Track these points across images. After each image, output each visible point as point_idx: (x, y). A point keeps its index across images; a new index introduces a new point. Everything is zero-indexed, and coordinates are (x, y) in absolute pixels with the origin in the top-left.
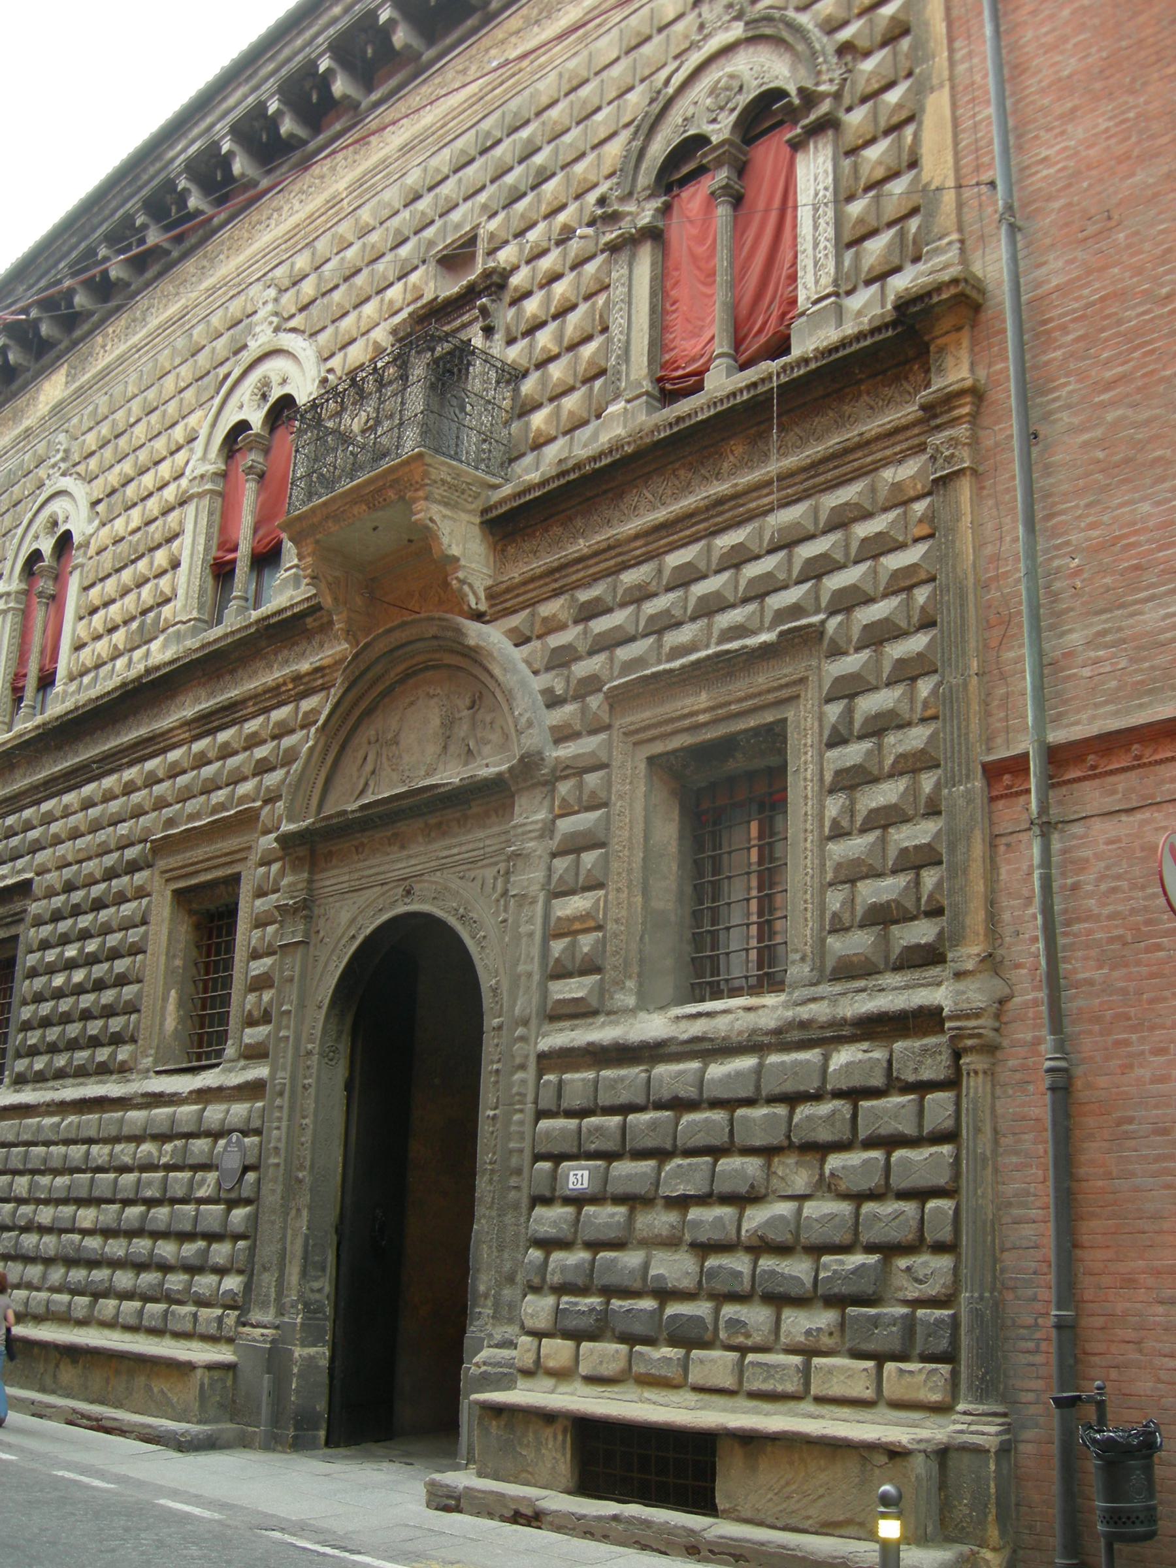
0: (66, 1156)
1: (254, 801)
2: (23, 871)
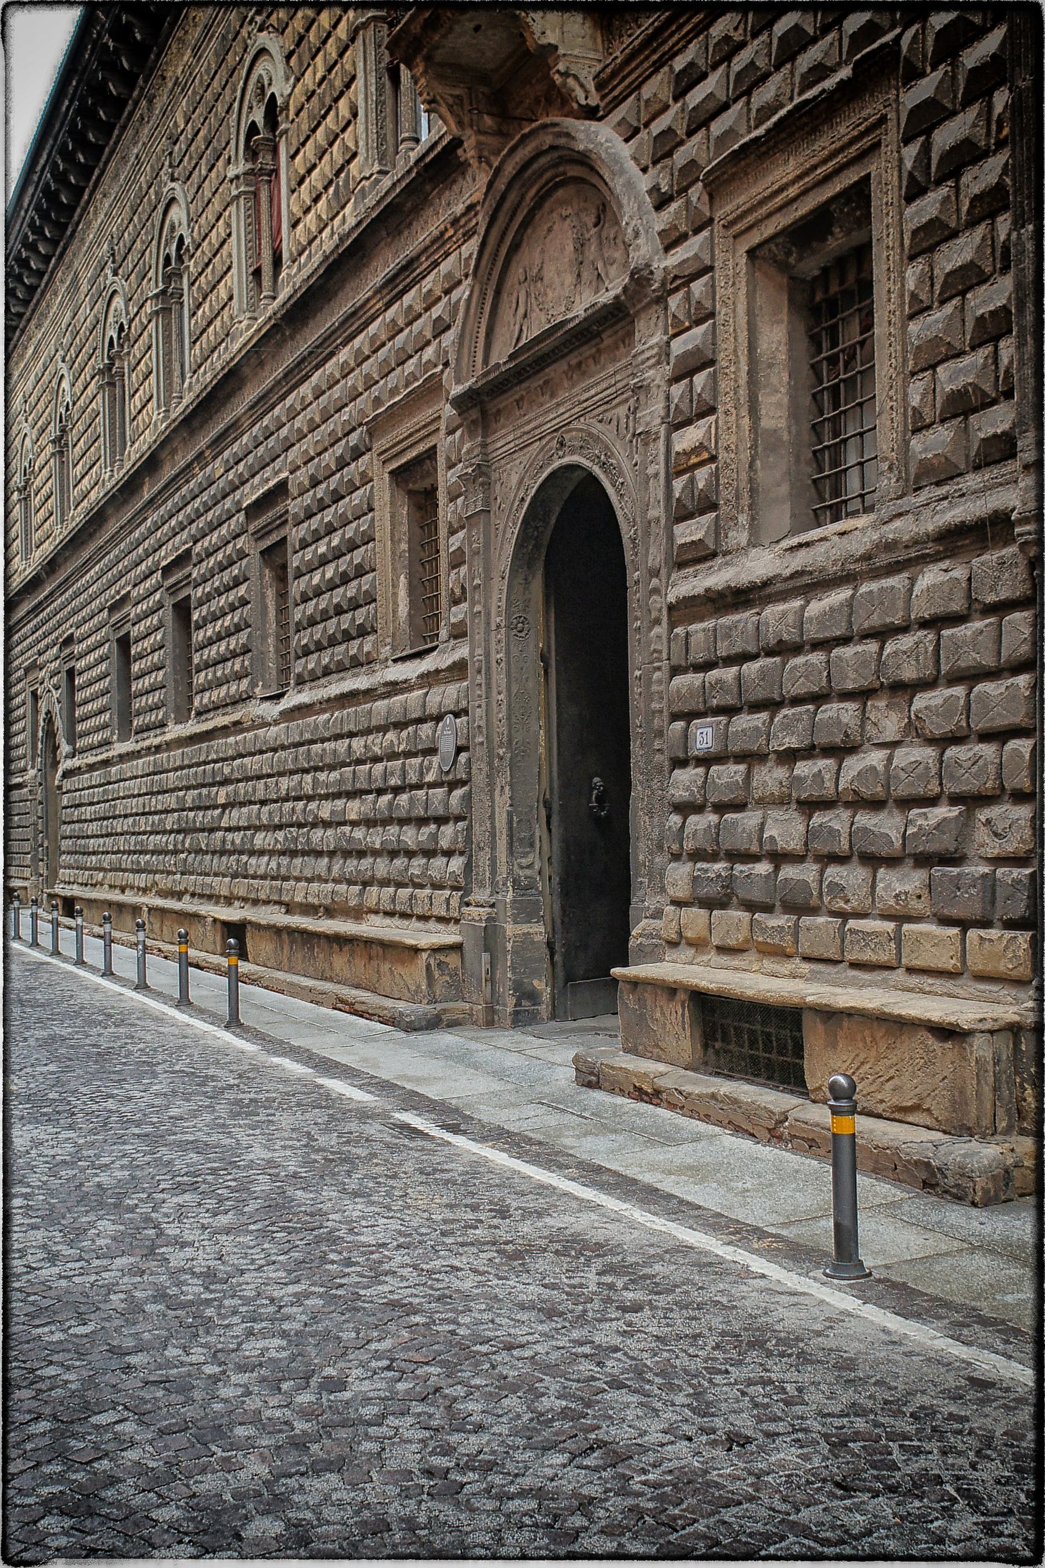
0: (335, 751)
1: (436, 366)
2: (280, 471)
